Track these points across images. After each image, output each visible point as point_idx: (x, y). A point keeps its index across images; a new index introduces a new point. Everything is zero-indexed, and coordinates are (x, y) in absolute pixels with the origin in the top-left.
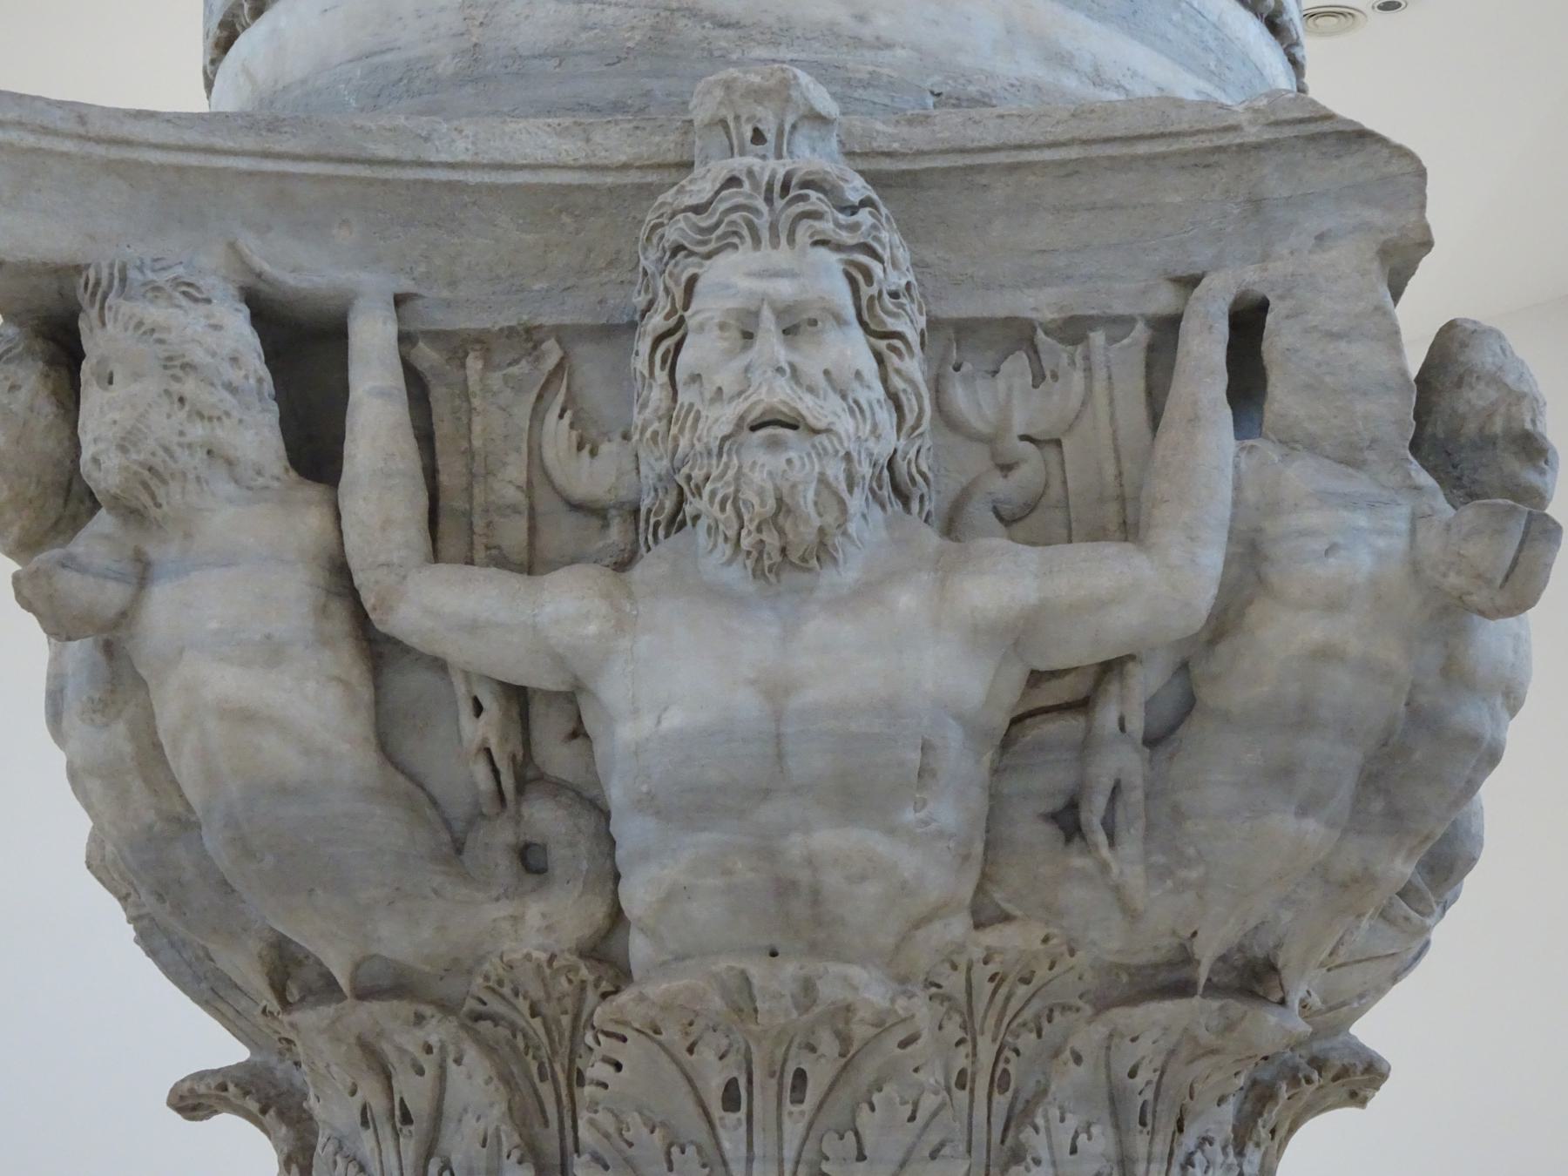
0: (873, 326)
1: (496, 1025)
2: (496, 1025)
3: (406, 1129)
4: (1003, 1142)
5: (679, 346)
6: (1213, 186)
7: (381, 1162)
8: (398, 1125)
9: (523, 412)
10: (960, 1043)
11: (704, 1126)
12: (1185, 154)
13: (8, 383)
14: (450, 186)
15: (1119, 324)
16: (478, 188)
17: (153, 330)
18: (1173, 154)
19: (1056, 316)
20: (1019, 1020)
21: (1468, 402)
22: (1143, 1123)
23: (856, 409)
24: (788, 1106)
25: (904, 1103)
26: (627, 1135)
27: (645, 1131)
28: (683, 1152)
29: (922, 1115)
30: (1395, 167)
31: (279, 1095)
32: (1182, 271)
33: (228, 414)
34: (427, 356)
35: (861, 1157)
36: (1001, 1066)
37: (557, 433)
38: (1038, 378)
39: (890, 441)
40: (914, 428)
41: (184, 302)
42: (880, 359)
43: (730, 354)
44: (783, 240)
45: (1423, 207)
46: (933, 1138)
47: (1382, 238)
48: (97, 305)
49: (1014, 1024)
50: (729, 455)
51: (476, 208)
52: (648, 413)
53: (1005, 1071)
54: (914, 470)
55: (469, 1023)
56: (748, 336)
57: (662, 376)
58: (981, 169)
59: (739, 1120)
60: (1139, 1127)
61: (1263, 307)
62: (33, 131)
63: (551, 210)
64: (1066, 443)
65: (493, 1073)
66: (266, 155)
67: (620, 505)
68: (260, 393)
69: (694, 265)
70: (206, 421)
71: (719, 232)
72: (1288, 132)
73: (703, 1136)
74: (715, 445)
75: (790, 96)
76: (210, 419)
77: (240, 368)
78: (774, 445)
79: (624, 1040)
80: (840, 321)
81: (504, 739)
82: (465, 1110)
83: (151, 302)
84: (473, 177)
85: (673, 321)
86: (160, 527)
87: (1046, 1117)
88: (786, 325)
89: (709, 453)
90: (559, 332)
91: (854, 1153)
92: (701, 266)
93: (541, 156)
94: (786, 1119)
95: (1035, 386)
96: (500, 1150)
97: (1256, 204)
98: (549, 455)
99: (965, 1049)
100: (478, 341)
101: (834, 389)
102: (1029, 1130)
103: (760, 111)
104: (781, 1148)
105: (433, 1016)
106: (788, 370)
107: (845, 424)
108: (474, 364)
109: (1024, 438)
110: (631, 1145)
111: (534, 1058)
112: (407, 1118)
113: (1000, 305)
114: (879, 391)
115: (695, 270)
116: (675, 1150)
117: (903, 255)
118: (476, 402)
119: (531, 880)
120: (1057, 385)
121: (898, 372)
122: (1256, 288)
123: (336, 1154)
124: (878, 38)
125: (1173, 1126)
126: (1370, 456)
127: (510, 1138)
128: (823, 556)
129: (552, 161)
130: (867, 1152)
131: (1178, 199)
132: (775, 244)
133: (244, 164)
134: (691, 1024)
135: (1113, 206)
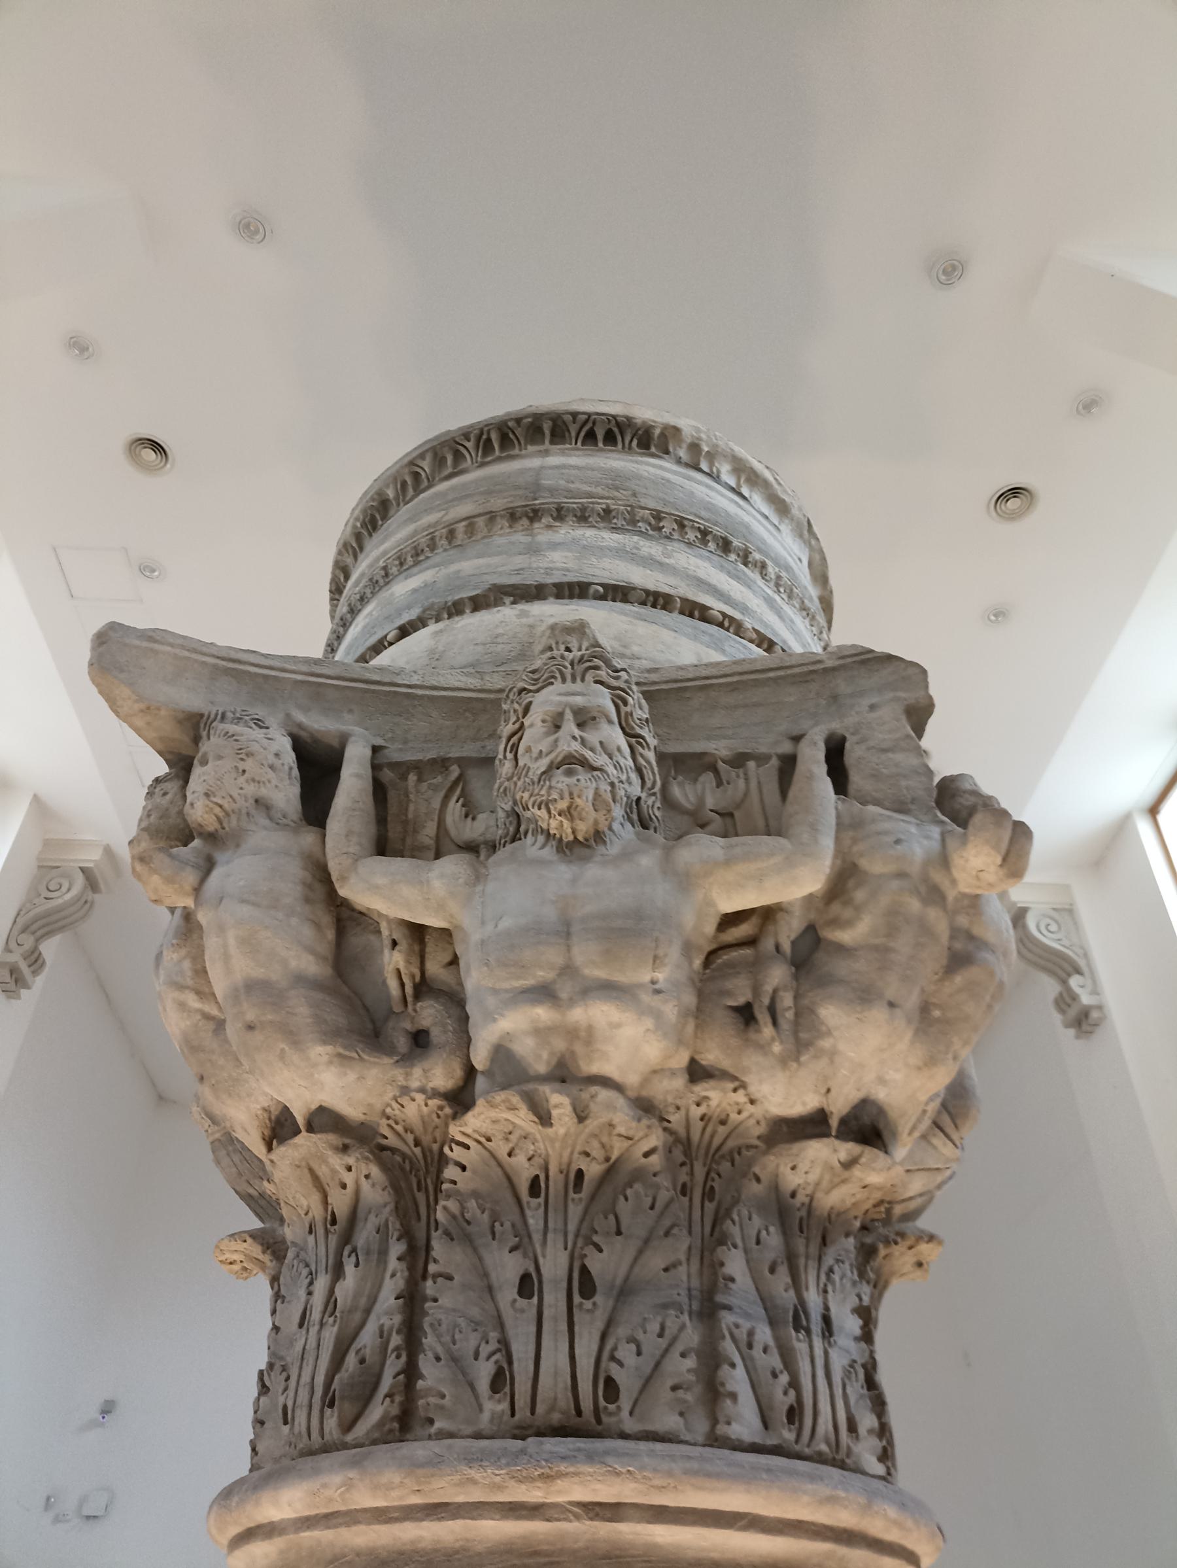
0: (627, 730)
1: (393, 1154)
2: (393, 1154)
3: (332, 1229)
4: (712, 1235)
5: (520, 739)
6: (810, 692)
7: (316, 1255)
8: (329, 1226)
9: (436, 804)
10: (683, 1164)
11: (516, 1209)
12: (794, 676)
13: (162, 792)
14: (407, 695)
15: (762, 759)
16: (422, 697)
17: (233, 735)
18: (788, 675)
19: (728, 753)
20: (720, 1153)
21: (960, 804)
22: (802, 1232)
23: (617, 766)
24: (571, 1195)
25: (646, 1196)
26: (467, 1216)
27: (478, 1212)
28: (502, 1226)
29: (659, 1205)
30: (910, 671)
31: (275, 1243)
32: (795, 733)
33: (269, 781)
34: (387, 775)
35: (619, 1233)
36: (709, 1183)
37: (455, 809)
38: (719, 784)
39: (636, 790)
40: (650, 789)
41: (253, 726)
42: (631, 747)
43: (548, 734)
44: (578, 679)
45: (927, 687)
46: (667, 1222)
47: (906, 703)
48: (207, 728)
49: (717, 1157)
50: (544, 781)
51: (421, 708)
52: (502, 779)
53: (712, 1188)
54: (651, 812)
55: (376, 1151)
56: (558, 727)
57: (510, 756)
58: (686, 688)
59: (539, 1204)
60: (799, 1233)
61: (843, 740)
62: (188, 650)
63: (460, 710)
64: (737, 814)
65: (387, 1184)
66: (313, 675)
67: (486, 843)
68: (290, 774)
69: (530, 697)
70: (256, 784)
71: (544, 678)
72: (849, 660)
73: (516, 1217)
74: (536, 780)
75: (585, 632)
76: (259, 782)
77: (280, 759)
78: (570, 773)
79: (468, 1147)
80: (610, 722)
81: (408, 962)
82: (370, 1212)
83: (236, 724)
84: (419, 692)
85: (517, 725)
86: (224, 843)
87: (739, 1215)
88: (578, 722)
89: (533, 783)
90: (460, 761)
91: (614, 1229)
92: (533, 697)
93: (457, 684)
94: (570, 1202)
95: (718, 787)
96: (388, 1234)
97: (835, 698)
98: (449, 820)
99: (685, 1169)
100: (416, 768)
101: (606, 753)
102: (729, 1222)
103: (569, 638)
104: (566, 1224)
105: (354, 1146)
106: (579, 739)
107: (611, 770)
108: (412, 778)
109: (712, 811)
110: (468, 1223)
111: (415, 1176)
112: (334, 1222)
113: (698, 747)
114: (631, 763)
115: (531, 699)
116: (497, 1224)
117: (647, 711)
118: (412, 797)
119: (419, 1050)
120: (730, 786)
121: (642, 755)
122: (838, 731)
123: (294, 1259)
124: (633, 655)
125: (819, 1239)
126: (913, 807)
127: (395, 1227)
128: (598, 840)
129: (463, 687)
130: (623, 1230)
131: (792, 699)
132: (574, 680)
133: (299, 677)
134: (510, 1133)
135: (757, 705)
